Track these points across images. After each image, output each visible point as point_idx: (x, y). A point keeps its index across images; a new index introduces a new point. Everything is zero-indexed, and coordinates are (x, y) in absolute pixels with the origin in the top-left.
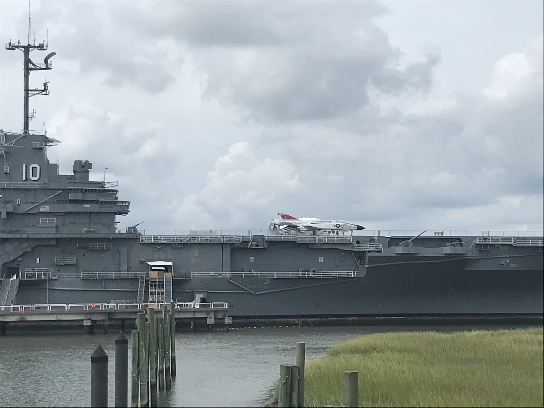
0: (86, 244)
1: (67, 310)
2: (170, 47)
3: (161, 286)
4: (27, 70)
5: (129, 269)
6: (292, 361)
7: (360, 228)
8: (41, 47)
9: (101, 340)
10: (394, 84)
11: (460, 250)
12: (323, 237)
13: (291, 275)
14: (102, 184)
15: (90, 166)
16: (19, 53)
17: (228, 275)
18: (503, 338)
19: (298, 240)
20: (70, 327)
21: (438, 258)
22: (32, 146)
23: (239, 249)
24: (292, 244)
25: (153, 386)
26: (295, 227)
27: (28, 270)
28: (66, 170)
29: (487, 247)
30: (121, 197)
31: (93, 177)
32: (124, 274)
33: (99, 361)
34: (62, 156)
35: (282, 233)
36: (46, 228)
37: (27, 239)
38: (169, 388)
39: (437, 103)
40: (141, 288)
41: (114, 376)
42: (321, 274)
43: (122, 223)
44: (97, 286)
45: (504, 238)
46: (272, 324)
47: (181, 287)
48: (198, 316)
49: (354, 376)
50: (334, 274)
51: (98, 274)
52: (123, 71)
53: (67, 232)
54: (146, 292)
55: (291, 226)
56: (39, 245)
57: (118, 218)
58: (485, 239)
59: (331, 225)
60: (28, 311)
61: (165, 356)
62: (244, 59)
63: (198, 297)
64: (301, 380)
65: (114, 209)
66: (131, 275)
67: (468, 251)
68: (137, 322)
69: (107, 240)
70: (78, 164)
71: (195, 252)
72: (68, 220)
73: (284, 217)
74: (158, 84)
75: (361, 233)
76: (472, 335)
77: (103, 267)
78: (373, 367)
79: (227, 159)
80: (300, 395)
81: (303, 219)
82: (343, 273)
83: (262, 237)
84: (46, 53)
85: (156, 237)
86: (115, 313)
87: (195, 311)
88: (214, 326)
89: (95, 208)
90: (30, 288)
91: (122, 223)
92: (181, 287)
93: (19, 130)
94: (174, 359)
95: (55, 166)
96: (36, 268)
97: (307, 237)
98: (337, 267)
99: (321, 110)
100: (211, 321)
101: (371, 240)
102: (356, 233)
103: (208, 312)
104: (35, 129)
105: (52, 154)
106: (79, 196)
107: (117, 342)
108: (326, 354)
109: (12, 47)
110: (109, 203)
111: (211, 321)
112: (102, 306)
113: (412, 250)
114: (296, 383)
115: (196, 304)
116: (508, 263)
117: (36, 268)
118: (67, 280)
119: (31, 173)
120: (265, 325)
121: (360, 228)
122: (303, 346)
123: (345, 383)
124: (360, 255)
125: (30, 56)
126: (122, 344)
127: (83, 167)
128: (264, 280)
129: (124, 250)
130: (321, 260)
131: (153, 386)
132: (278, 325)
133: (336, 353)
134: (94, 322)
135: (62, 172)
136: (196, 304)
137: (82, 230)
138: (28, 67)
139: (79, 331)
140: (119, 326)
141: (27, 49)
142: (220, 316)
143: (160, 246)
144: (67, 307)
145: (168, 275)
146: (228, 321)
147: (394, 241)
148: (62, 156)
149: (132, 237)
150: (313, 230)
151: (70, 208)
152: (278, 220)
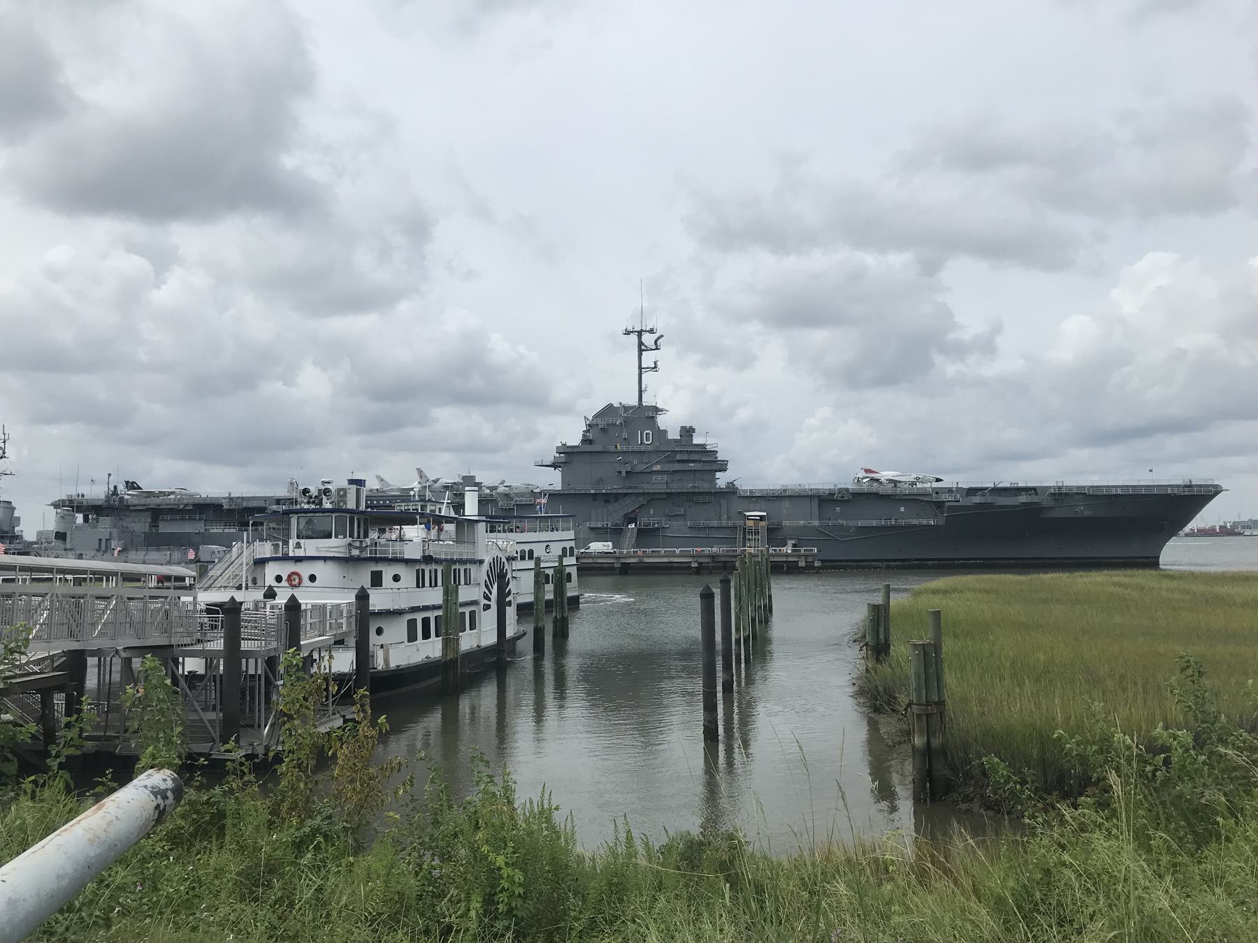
0: (691, 497)
1: (677, 553)
2: (754, 327)
3: (757, 533)
4: (640, 351)
5: (729, 518)
6: (878, 599)
7: (938, 480)
8: (651, 331)
9: (705, 579)
10: (959, 351)
11: (1035, 499)
12: (905, 488)
13: (874, 523)
14: (703, 446)
15: (694, 430)
16: (634, 337)
17: (816, 523)
18: (1080, 580)
19: (881, 492)
20: (680, 568)
21: (1014, 506)
22: (645, 415)
23: (826, 500)
24: (875, 495)
25: (753, 620)
26: (877, 480)
27: (644, 520)
28: (674, 435)
29: (1061, 496)
30: (720, 457)
31: (697, 440)
32: (724, 523)
33: (707, 597)
34: (671, 423)
35: (865, 486)
36: (658, 484)
37: (643, 494)
38: (767, 621)
39: (1006, 363)
40: (740, 536)
41: (552, 678)
42: (903, 522)
43: (722, 480)
44: (703, 534)
45: (1078, 487)
46: (857, 567)
47: (775, 534)
48: (790, 559)
49: (937, 614)
50: (915, 522)
51: (702, 523)
52: (713, 354)
53: (676, 487)
54: (744, 538)
55: (873, 479)
56: (653, 498)
57: (718, 475)
58: (1060, 488)
59: (911, 478)
60: (645, 555)
61: (762, 593)
62: (818, 336)
63: (790, 543)
64: (887, 618)
65: (715, 467)
66: (730, 523)
67: (1044, 500)
68: (737, 564)
69: (710, 493)
70: (683, 428)
71: (787, 504)
72: (677, 477)
73: (867, 471)
74: (745, 362)
75: (940, 485)
76: (1048, 577)
77: (707, 517)
78: (954, 606)
79: (813, 421)
80: (887, 630)
81: (884, 473)
82: (924, 522)
83: (847, 490)
84: (654, 336)
85: (751, 491)
86: (719, 556)
87: (787, 555)
88: (806, 568)
89: (698, 466)
90: (645, 535)
91: (722, 480)
92: (775, 534)
93: (635, 402)
94: (770, 597)
95: (665, 432)
96: (651, 518)
97: (889, 489)
98: (918, 516)
99: (888, 379)
100: (802, 564)
101: (950, 490)
102: (935, 485)
103: (799, 556)
104: (647, 401)
105: (662, 421)
106: (685, 457)
107: (722, 581)
108: (911, 595)
109: (628, 333)
110: (710, 462)
111: (802, 564)
112: (707, 550)
113: (989, 499)
114: (882, 619)
115: (788, 549)
116: (1082, 511)
117: (651, 518)
118: (677, 528)
119: (645, 439)
120: (851, 568)
121: (938, 480)
122: (888, 587)
123: (930, 620)
124: (940, 505)
125: (643, 340)
126: (725, 583)
127: (688, 432)
128: (850, 528)
129: (724, 502)
130: (902, 509)
131: (753, 620)
132: (863, 568)
133: (917, 594)
134: (700, 564)
135: (670, 437)
136: (788, 549)
137: (688, 485)
138: (641, 348)
139: (619, 598)
140: (723, 567)
141: (640, 333)
142: (810, 559)
143: (755, 499)
144: (678, 551)
145: (763, 524)
146: (817, 564)
147: (972, 491)
148: (671, 423)
149: (731, 491)
150: (895, 482)
151: (677, 467)
152: (861, 474)
